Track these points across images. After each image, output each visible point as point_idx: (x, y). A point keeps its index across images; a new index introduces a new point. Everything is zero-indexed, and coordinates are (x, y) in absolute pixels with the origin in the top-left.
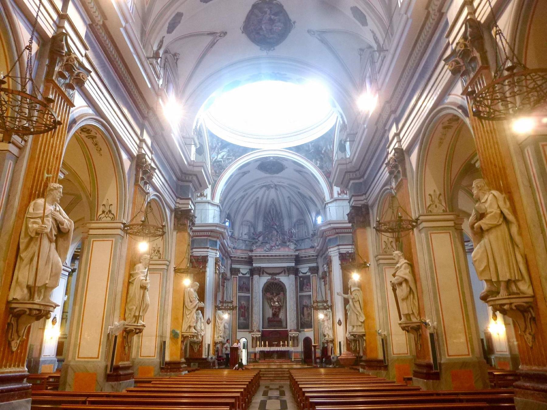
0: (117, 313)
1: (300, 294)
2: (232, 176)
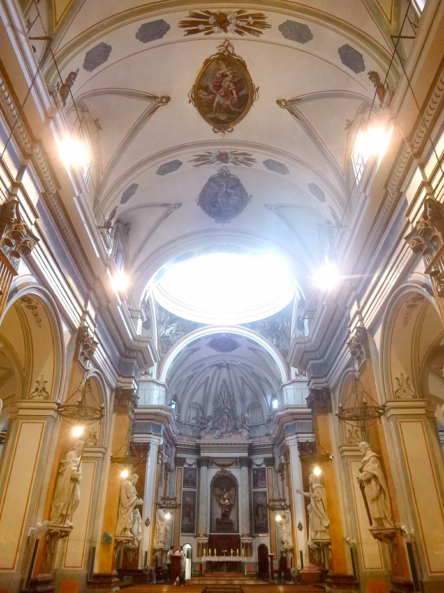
1: (254, 490)
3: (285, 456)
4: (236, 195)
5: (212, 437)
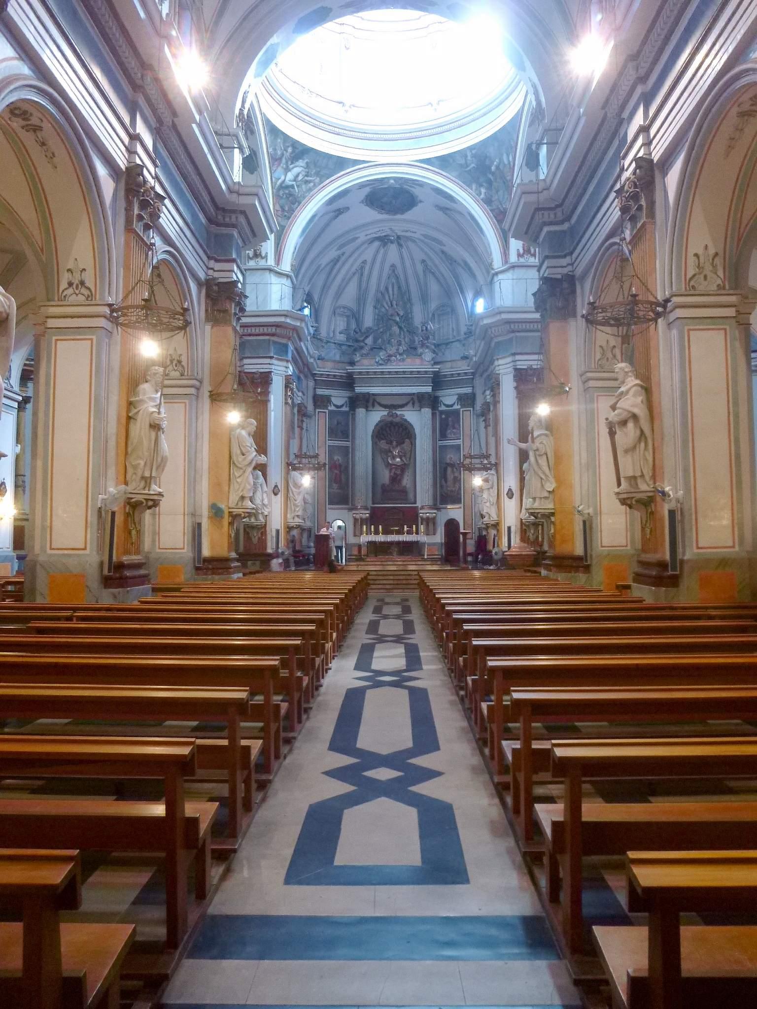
0: (112, 472)
1: (440, 443)
2: (314, 217)
3: (492, 391)
5: (373, 362)
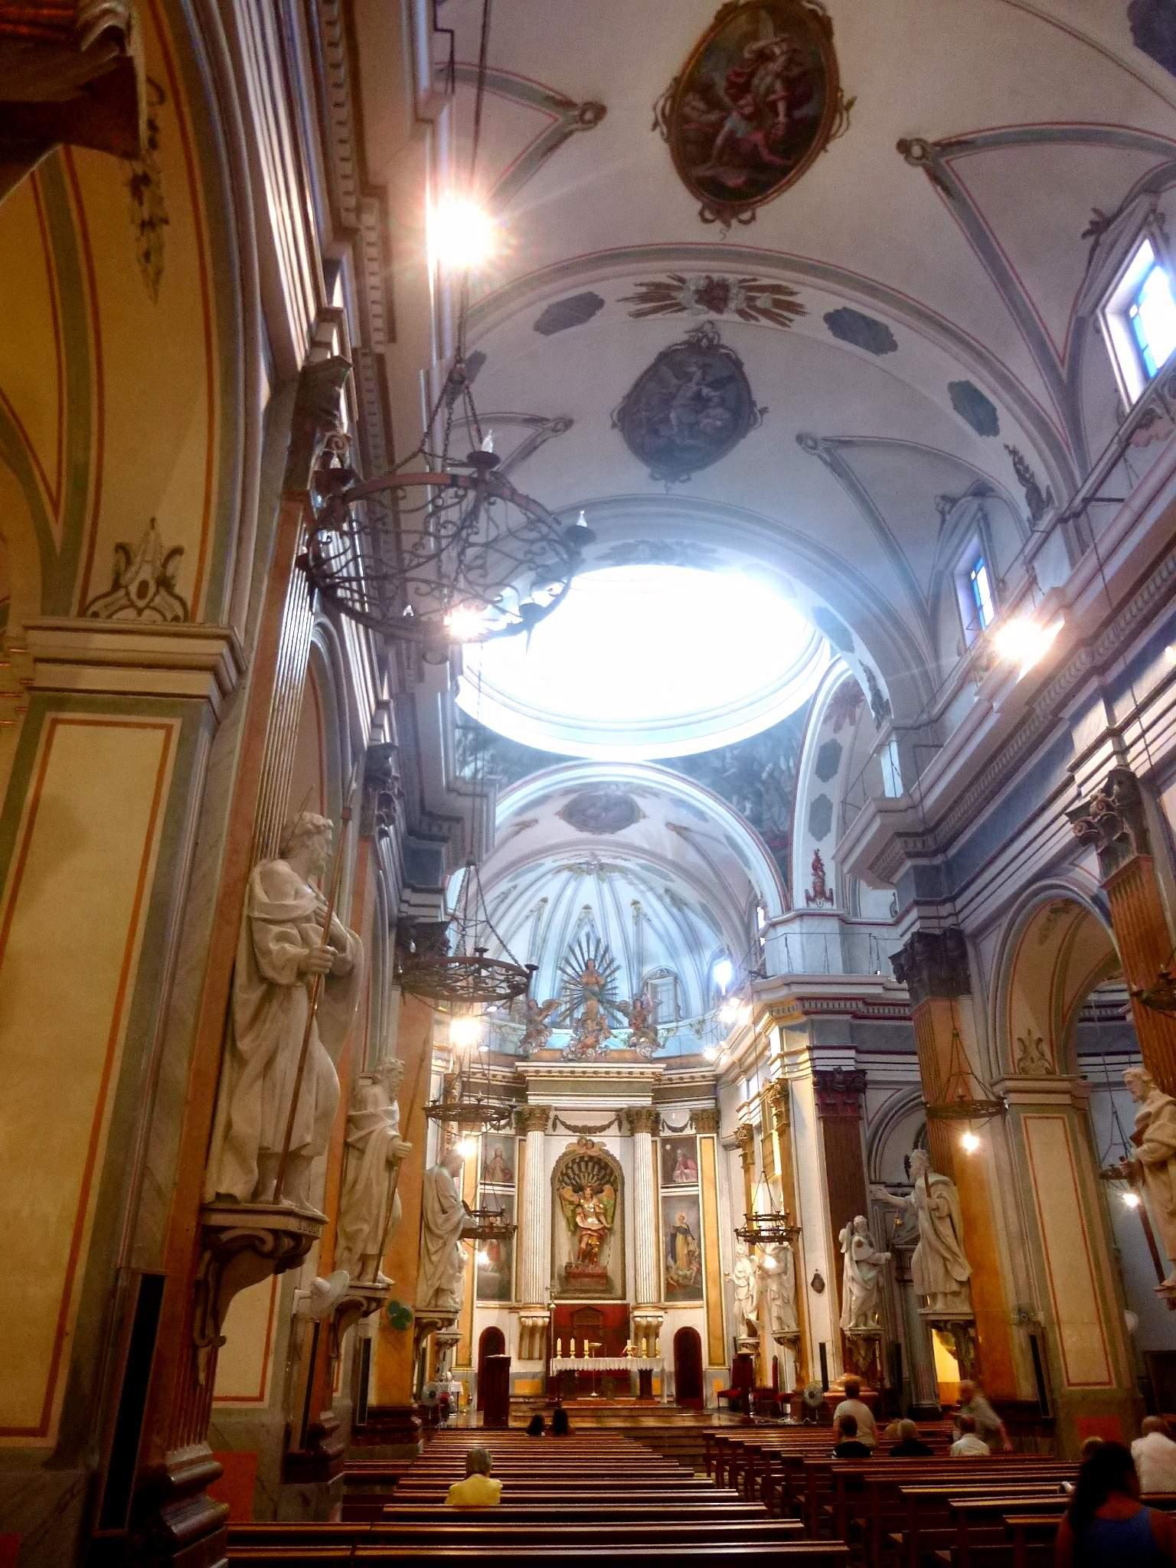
4: (722, 403)
